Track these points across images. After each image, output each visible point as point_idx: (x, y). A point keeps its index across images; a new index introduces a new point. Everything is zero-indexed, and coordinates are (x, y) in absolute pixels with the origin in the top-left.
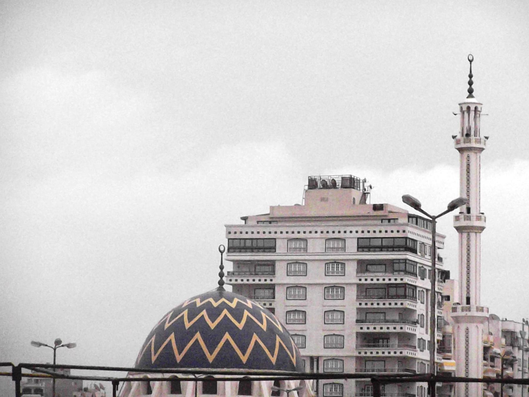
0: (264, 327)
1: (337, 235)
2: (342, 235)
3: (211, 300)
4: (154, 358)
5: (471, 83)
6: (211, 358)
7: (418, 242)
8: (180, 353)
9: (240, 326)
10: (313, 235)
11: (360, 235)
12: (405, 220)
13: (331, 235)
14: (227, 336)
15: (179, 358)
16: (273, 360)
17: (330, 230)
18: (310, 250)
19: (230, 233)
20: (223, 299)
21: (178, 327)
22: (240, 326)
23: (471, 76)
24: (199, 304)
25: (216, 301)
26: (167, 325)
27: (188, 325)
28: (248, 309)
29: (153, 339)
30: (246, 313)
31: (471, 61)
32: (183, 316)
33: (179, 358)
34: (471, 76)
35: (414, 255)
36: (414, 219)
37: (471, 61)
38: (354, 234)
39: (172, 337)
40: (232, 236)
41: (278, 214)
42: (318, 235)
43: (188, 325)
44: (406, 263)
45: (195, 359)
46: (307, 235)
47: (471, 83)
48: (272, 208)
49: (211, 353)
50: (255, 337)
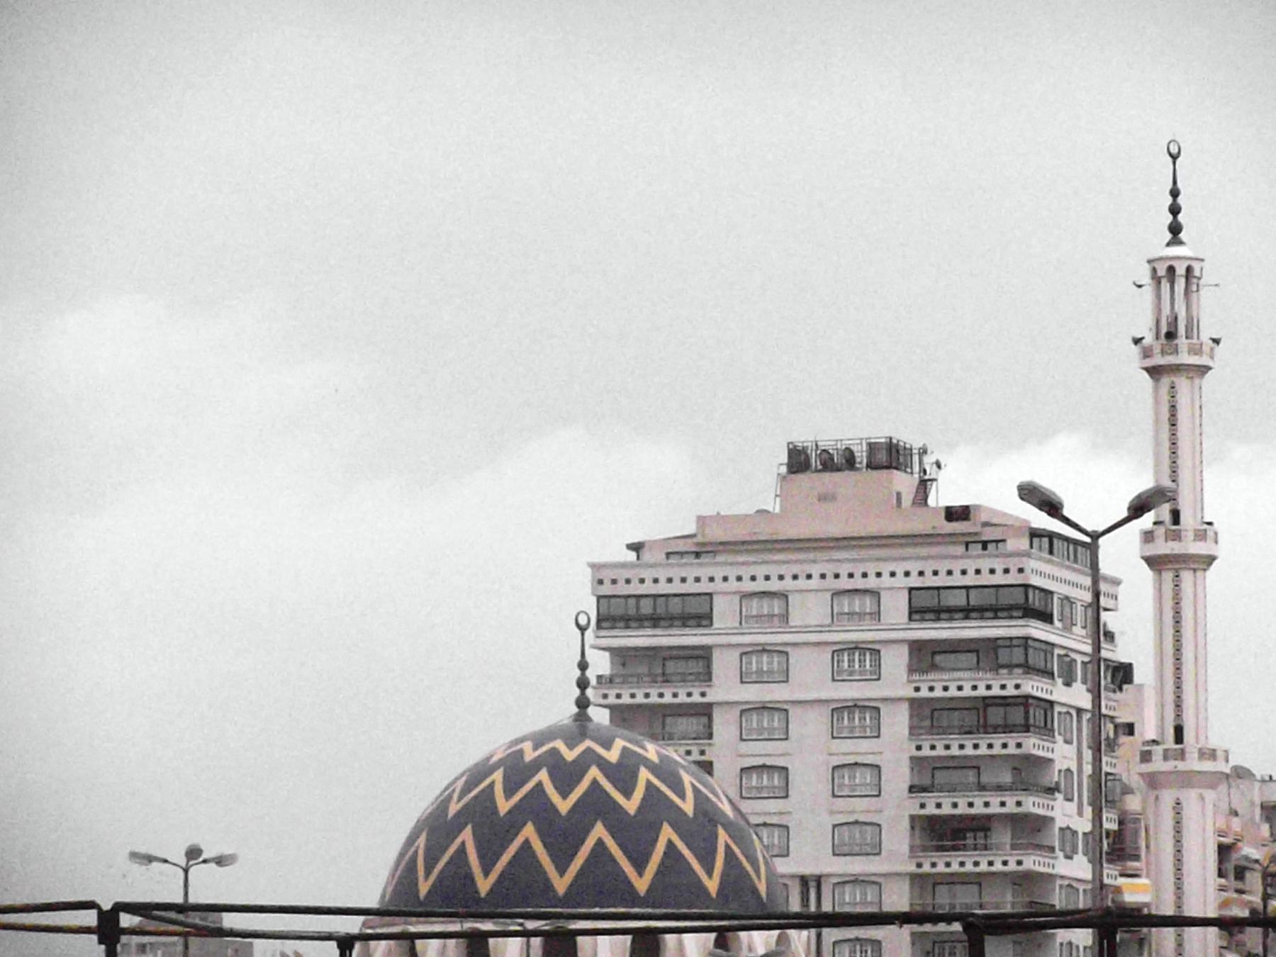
0: (688, 807)
1: (859, 583)
2: (872, 582)
3: (559, 745)
4: (424, 888)
5: (1175, 210)
7: (1079, 604)
8: (486, 873)
9: (631, 806)
10: (802, 583)
12: (1024, 543)
13: (845, 583)
17: (844, 570)
18: (795, 620)
19: (601, 582)
20: (588, 743)
21: (479, 812)
22: (631, 806)
23: (1175, 193)
24: (530, 755)
25: (571, 747)
26: (454, 808)
27: (504, 806)
29: (422, 841)
30: (644, 775)
31: (1174, 158)
32: (492, 785)
34: (1175, 193)
35: (1047, 627)
36: (1046, 540)
37: (1174, 158)
38: (901, 581)
39: (467, 835)
40: (607, 589)
42: (815, 583)
43: (504, 806)
46: (788, 584)
47: (1175, 210)
48: (701, 520)
50: (667, 833)
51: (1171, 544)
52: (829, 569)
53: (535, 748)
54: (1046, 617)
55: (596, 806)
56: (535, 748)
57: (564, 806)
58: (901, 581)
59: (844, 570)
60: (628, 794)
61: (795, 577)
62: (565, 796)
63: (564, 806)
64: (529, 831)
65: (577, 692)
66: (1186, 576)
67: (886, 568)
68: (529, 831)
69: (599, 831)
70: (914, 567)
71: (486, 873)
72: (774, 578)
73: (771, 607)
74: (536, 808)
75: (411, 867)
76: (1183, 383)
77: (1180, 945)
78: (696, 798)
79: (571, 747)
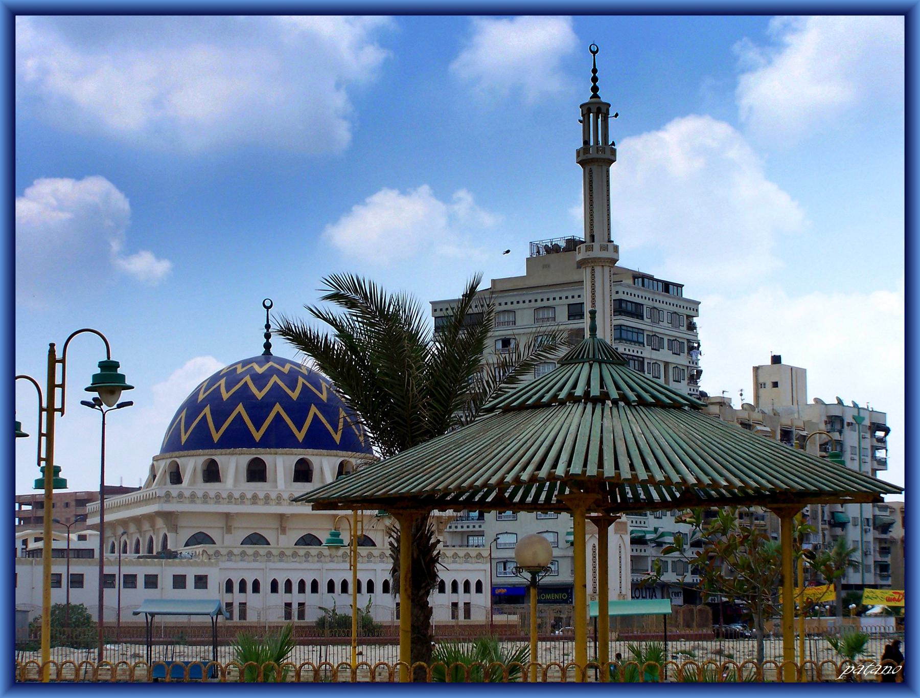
0: (324, 397)
1: (545, 303)
2: (551, 303)
3: (256, 367)
4: (184, 438)
5: (595, 79)
6: (257, 436)
7: (665, 312)
8: (217, 430)
9: (295, 395)
10: (521, 305)
11: (572, 301)
12: (630, 282)
13: (539, 304)
14: (278, 408)
15: (216, 437)
16: (337, 438)
17: (539, 298)
18: (518, 323)
19: (435, 310)
20: (271, 364)
21: (214, 398)
22: (295, 395)
23: (595, 71)
24: (239, 371)
25: (261, 366)
26: (201, 397)
27: (225, 396)
28: (304, 376)
29: (183, 414)
30: (301, 380)
31: (594, 53)
32: (219, 386)
33: (216, 437)
34: (595, 71)
35: (640, 321)
36: (640, 280)
37: (594, 53)
38: (564, 301)
39: (207, 410)
40: (439, 314)
41: (499, 287)
42: (527, 304)
43: (225, 396)
44: (621, 329)
45: (237, 438)
46: (515, 306)
47: (595, 79)
48: (493, 281)
49: (258, 429)
50: (313, 409)
51: (589, 253)
52: (533, 298)
53: (243, 367)
54: (641, 317)
55: (277, 395)
56: (243, 367)
57: (260, 395)
58: (564, 301)
59: (539, 298)
60: (293, 390)
61: (518, 302)
62: (260, 390)
63: (260, 395)
64: (240, 408)
65: (265, 340)
66: (598, 270)
67: (557, 296)
68: (240, 408)
69: (278, 408)
70: (570, 294)
71: (217, 430)
72: (509, 303)
73: (508, 317)
74: (243, 395)
75: (178, 429)
76: (595, 168)
77: (585, 465)
78: (328, 394)
79: (261, 366)
